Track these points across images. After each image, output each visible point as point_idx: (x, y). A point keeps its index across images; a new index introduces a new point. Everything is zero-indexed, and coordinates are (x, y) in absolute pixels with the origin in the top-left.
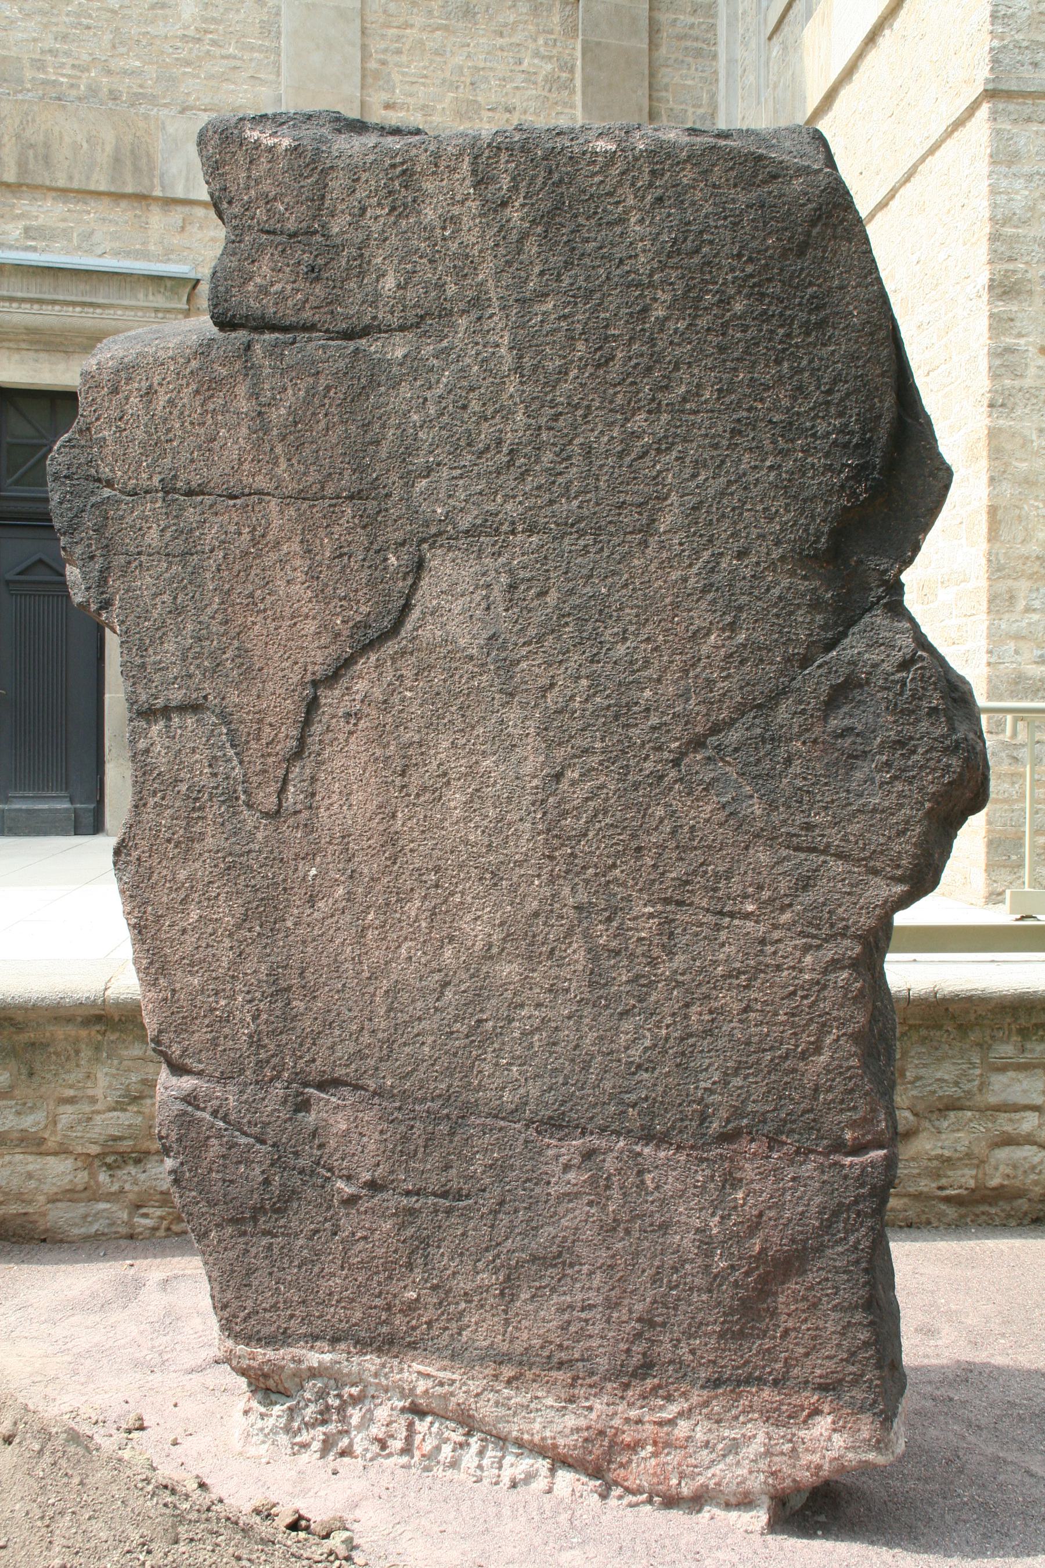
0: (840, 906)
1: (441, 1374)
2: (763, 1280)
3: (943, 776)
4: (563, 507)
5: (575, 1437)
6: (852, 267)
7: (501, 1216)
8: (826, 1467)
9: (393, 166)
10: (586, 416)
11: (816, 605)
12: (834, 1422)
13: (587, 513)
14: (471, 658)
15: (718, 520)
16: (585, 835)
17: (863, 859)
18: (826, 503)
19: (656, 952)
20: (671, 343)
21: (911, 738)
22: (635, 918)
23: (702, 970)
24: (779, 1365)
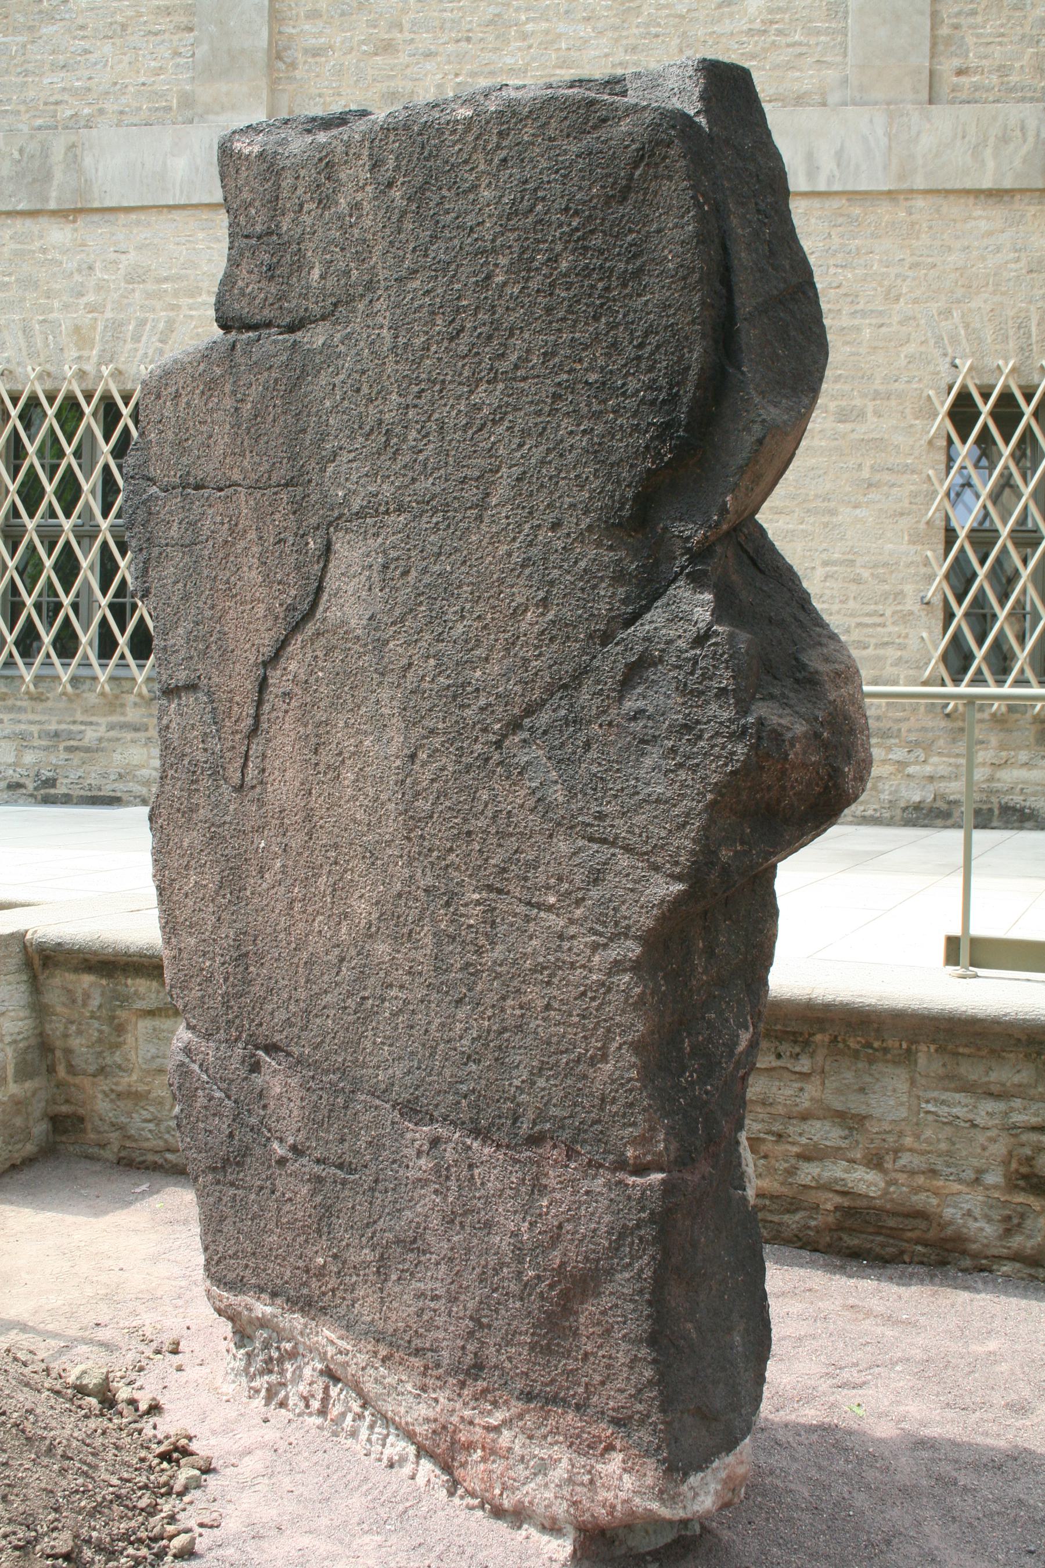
0: (623, 903)
1: (340, 1342)
2: (564, 1295)
3: (726, 765)
4: (425, 484)
5: (426, 1427)
6: (671, 207)
7: (377, 1194)
8: (619, 1507)
9: (321, 160)
10: (441, 391)
11: (620, 577)
12: (624, 1461)
13: (438, 490)
14: (358, 638)
15: (538, 491)
16: (431, 817)
17: (646, 853)
18: (631, 466)
19: (482, 941)
20: (508, 309)
21: (698, 722)
22: (466, 905)
23: (515, 962)
24: (581, 1390)
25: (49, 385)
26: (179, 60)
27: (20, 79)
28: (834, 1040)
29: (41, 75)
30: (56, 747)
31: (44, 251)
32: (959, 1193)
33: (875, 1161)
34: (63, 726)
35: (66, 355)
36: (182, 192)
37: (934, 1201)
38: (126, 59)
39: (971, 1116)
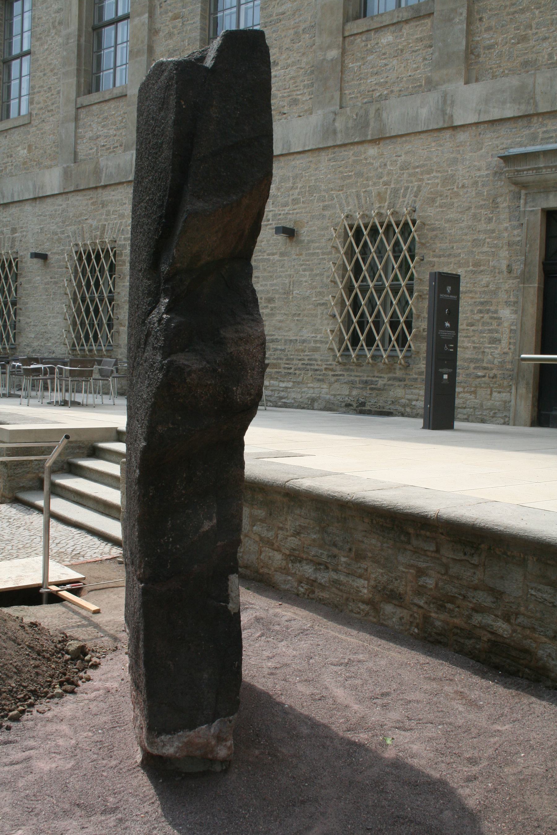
25: (366, 221)
26: (427, 62)
27: (358, 82)
28: (489, 548)
29: (367, 79)
30: (366, 388)
31: (366, 159)
32: (545, 643)
33: (507, 618)
34: (370, 378)
35: (374, 206)
36: (425, 124)
37: (534, 645)
38: (403, 65)
39: (552, 600)
